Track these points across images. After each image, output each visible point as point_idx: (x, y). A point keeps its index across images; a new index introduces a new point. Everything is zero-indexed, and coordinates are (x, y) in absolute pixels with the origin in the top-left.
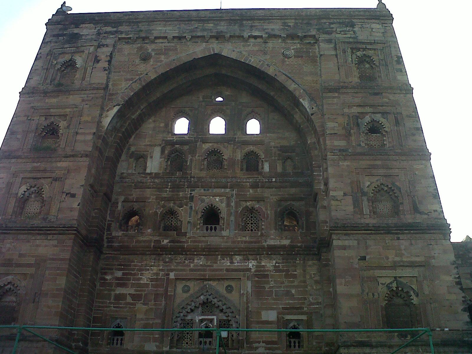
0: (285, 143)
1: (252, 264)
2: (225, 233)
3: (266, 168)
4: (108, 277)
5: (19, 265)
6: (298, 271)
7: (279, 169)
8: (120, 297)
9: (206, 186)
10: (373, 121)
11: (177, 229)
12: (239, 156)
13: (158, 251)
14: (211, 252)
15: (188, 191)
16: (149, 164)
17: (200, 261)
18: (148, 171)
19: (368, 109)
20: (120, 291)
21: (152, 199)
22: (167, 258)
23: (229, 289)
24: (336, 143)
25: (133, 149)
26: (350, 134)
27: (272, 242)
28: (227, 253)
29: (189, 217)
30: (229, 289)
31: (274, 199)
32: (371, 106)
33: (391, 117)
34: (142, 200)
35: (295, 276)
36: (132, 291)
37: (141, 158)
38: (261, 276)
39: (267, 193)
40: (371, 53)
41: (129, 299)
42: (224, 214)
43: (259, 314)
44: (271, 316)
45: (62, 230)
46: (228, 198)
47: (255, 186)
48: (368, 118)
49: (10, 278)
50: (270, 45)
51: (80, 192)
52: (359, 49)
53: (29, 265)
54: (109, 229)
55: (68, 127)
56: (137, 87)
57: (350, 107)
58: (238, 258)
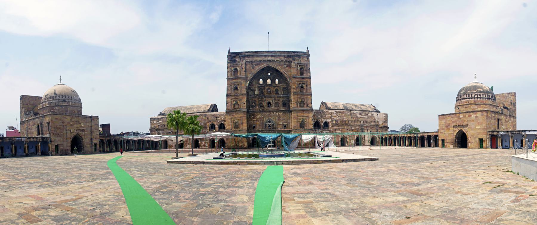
9: (268, 97)
12: (274, 90)
13: (260, 112)
14: (270, 111)
17: (268, 113)
28: (273, 112)
29: (265, 104)
37: (254, 91)
38: (279, 116)
39: (280, 99)
44: (281, 123)
45: (244, 111)
47: (278, 97)
51: (245, 102)
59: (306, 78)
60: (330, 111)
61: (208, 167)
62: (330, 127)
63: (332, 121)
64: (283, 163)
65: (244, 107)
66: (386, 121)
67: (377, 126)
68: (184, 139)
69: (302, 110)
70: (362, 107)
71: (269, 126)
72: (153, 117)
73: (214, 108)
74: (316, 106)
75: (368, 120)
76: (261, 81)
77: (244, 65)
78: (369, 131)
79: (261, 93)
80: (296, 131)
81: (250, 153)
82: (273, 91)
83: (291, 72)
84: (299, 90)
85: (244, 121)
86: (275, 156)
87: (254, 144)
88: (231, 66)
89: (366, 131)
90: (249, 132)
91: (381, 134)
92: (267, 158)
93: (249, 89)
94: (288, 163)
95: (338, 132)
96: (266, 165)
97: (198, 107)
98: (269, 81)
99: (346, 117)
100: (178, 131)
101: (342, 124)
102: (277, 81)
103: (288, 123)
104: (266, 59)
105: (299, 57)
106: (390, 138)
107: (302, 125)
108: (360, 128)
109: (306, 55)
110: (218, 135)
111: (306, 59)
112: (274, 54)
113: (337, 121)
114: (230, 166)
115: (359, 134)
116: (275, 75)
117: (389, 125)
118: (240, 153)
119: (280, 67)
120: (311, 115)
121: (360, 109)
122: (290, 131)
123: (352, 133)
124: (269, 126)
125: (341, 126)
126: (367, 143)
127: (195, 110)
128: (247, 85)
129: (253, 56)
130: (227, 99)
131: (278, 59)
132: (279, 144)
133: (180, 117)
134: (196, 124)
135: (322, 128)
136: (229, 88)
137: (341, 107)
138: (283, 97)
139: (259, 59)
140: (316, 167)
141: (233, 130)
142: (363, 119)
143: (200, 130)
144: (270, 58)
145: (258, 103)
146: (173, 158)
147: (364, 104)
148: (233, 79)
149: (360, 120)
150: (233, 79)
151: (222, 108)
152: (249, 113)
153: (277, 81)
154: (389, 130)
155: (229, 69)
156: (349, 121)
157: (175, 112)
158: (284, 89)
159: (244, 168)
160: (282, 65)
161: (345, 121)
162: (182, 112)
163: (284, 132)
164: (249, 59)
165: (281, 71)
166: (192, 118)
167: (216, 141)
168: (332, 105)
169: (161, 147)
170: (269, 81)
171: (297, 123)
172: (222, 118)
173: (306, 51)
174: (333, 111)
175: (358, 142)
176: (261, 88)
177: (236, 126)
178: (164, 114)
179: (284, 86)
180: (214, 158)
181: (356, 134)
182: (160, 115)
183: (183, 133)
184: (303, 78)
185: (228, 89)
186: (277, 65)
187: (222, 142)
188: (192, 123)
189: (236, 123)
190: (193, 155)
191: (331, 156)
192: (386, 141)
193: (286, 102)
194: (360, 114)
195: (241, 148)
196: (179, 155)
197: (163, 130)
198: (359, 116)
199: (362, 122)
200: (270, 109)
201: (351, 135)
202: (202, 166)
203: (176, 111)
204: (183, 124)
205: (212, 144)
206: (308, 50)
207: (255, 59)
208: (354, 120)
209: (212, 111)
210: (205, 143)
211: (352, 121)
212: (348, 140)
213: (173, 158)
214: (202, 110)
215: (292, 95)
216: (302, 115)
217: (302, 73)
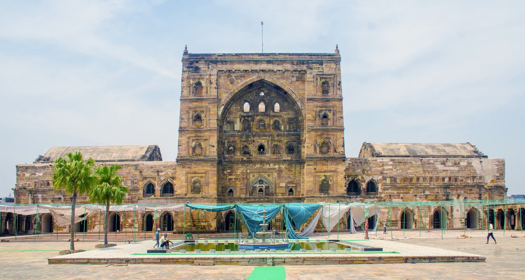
0: (290, 116)
1: (277, 167)
2: (267, 155)
3: (283, 128)
4: (225, 172)
5: (199, 173)
6: (293, 169)
7: (288, 128)
8: (230, 179)
9: (259, 136)
10: (325, 113)
11: (248, 153)
12: (272, 122)
13: (243, 162)
14: (262, 162)
15: (252, 138)
16: (235, 126)
17: (258, 166)
18: (235, 129)
19: (324, 109)
20: (230, 177)
21: (238, 141)
22: (246, 165)
23: (269, 175)
24: (310, 124)
25: (228, 119)
26: (316, 120)
27: (284, 159)
28: (268, 163)
29: (253, 149)
30: (269, 175)
31: (286, 141)
32: (325, 107)
33: (332, 112)
34: (234, 142)
35: (292, 171)
36: (234, 177)
37: (232, 123)
38: (280, 171)
39: (283, 139)
40: (328, 80)
41: (234, 180)
42: (266, 147)
43: (279, 184)
44: (283, 185)
45: (212, 160)
46: (268, 141)
47: (278, 135)
48: (323, 113)
49: (197, 178)
50: (286, 74)
51: (216, 145)
52: (323, 78)
53: (203, 173)
54: (223, 154)
55: (206, 117)
56: (230, 97)
57: (317, 107)
58: (272, 165)
59: (334, 100)
60: (379, 160)
61: (135, 269)
62: (380, 190)
63: (384, 178)
64: (284, 262)
65: (213, 152)
66: (501, 175)
67: (480, 186)
68: (90, 213)
69: (325, 159)
70: (447, 149)
71: (261, 190)
72: (22, 163)
73: (154, 154)
74: (352, 151)
75: (460, 174)
76: (247, 107)
77: (214, 78)
78: (461, 198)
79: (247, 128)
80: (312, 198)
81: (221, 241)
82: (269, 125)
83: (304, 89)
84: (318, 122)
85: (210, 180)
86: (269, 247)
87: (228, 223)
88: (188, 78)
89: (455, 198)
90: (220, 199)
91: (488, 203)
92: (254, 252)
93: (224, 119)
94: (296, 261)
95: (396, 202)
96: (253, 264)
97: (122, 150)
98: (262, 107)
99: (414, 170)
100: (75, 195)
101: (406, 185)
102: (277, 107)
103: (298, 185)
104: (257, 67)
105: (321, 63)
106: (511, 212)
107: (324, 187)
108: (441, 192)
109: (335, 59)
110: (158, 207)
111: (333, 66)
112: (271, 59)
113: (394, 179)
114: (179, 266)
115: (440, 203)
116: (273, 95)
117: (508, 183)
118: (202, 241)
119: (282, 81)
120: (341, 168)
121: (442, 153)
122: (300, 200)
123: (424, 202)
124: (261, 190)
125: (402, 188)
126: (458, 224)
127: (115, 156)
128: (220, 113)
129: (232, 62)
130: (180, 136)
131: (280, 68)
132: (278, 224)
133: (81, 167)
134: (115, 183)
135: (363, 194)
136: (185, 117)
137: (403, 151)
138: (288, 135)
139: (243, 67)
140: (350, 271)
141: (189, 195)
142: (449, 174)
143: (123, 195)
144: (264, 66)
145: (239, 145)
146: (62, 253)
147: (452, 143)
148: (192, 101)
149: (443, 174)
150: (192, 101)
151: (170, 154)
152: (223, 163)
153: (277, 107)
154: (509, 194)
155: (185, 84)
156: (418, 179)
157: (70, 155)
158: (290, 121)
159: (207, 272)
160: (287, 78)
161: (411, 179)
162: (86, 157)
163: (289, 200)
164: (225, 67)
165: (286, 89)
166: (105, 170)
167: (156, 217)
168: (384, 149)
169: (40, 228)
170: (262, 107)
171: (315, 184)
172: (170, 172)
173: (333, 51)
174: (386, 160)
175: (437, 221)
176: (246, 119)
177: (196, 189)
178: (48, 160)
179: (291, 114)
180: (149, 252)
181: (434, 205)
182: (39, 160)
183: (88, 199)
184: (328, 100)
185: (182, 119)
186: (278, 79)
187: (168, 221)
188: (107, 180)
189: (195, 182)
190: (106, 245)
191: (381, 250)
192: (500, 218)
193: (294, 144)
194: (443, 163)
195: (204, 231)
196: (77, 246)
197: (44, 192)
198: (440, 167)
199: (447, 180)
200: (263, 157)
201: (422, 206)
202: (124, 267)
203: (74, 154)
204: (88, 182)
205: (148, 222)
206: (337, 50)
207: (236, 67)
208: (430, 175)
209: (151, 158)
210: (133, 221)
211: (424, 179)
212: (416, 217)
213: (62, 253)
214: (129, 155)
215: (305, 132)
216: (325, 168)
217: (325, 92)
